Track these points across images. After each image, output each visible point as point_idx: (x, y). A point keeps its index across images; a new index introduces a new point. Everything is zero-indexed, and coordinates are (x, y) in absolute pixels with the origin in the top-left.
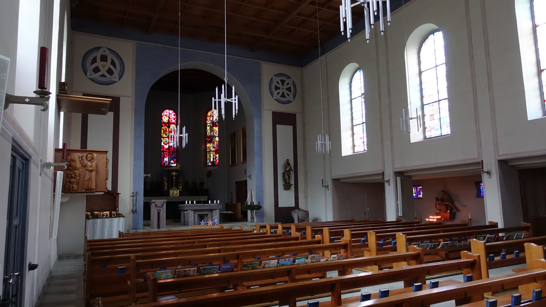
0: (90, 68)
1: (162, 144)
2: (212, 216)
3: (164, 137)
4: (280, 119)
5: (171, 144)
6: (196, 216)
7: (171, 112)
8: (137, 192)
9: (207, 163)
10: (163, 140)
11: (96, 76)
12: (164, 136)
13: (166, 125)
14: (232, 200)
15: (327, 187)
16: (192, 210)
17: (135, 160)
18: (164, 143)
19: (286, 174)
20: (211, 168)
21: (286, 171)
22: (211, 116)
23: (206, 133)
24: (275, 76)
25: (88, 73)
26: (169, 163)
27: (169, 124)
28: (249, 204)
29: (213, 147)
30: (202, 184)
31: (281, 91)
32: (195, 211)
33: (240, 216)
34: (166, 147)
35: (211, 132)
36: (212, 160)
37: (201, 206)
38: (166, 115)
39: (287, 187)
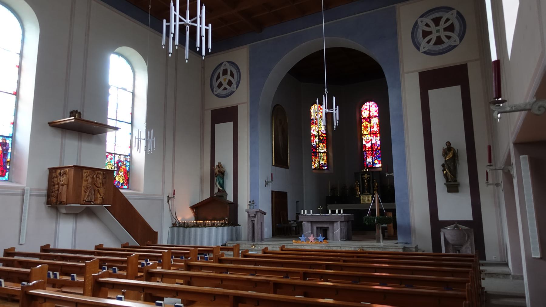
0: (216, 84)
1: (364, 143)
3: (365, 135)
4: (430, 80)
5: (373, 142)
6: (315, 229)
7: (371, 103)
8: (253, 201)
11: (220, 91)
12: (365, 133)
13: (366, 120)
15: (497, 185)
16: (308, 222)
17: (251, 166)
18: (366, 142)
19: (451, 166)
21: (445, 161)
24: (458, 13)
25: (214, 90)
26: (373, 163)
27: (370, 118)
31: (434, 37)
32: (312, 222)
34: (369, 145)
37: (323, 217)
38: (366, 109)
39: (453, 187)
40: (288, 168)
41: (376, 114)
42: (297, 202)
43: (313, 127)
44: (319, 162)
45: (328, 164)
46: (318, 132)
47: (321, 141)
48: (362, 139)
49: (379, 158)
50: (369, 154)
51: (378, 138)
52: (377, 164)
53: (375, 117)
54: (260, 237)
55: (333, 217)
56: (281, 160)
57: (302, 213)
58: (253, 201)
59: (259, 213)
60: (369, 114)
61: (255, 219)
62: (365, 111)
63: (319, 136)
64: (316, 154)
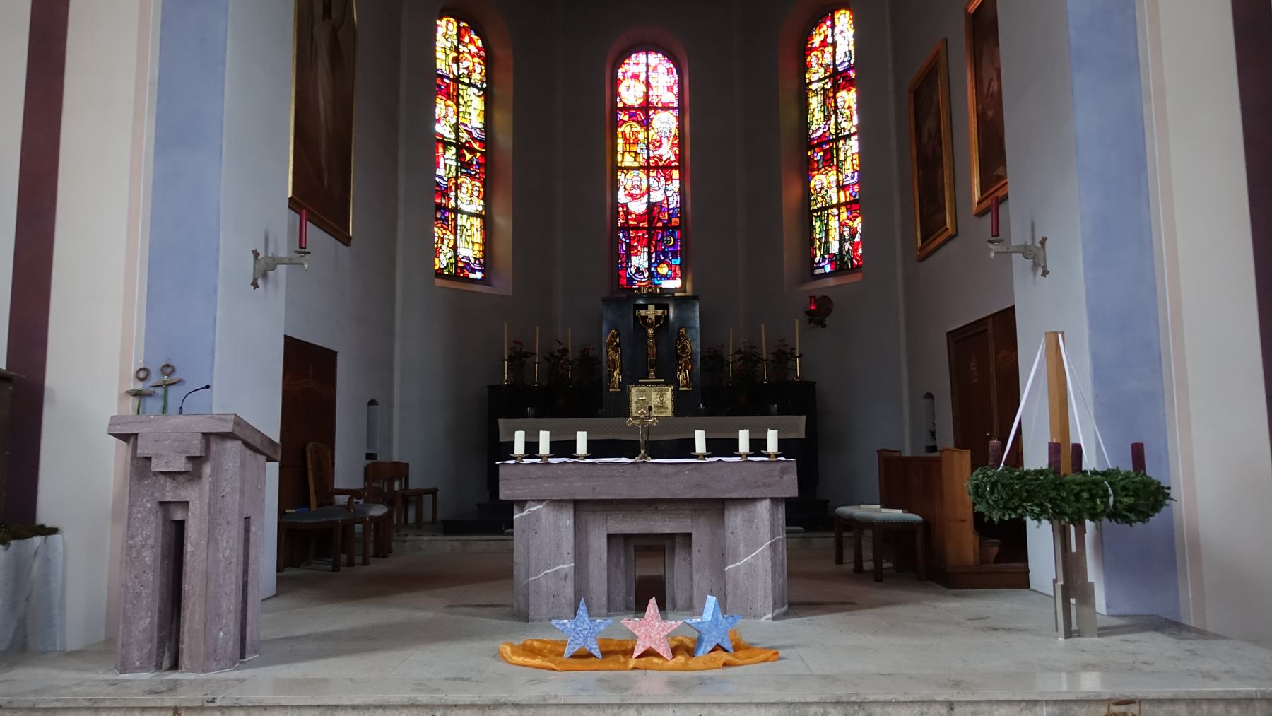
1: (622, 197)
2: (721, 557)
3: (629, 169)
5: (657, 197)
6: (598, 544)
7: (655, 59)
8: (168, 369)
9: (812, 265)
10: (625, 180)
12: (628, 161)
14: (933, 434)
16: (558, 503)
20: (831, 282)
22: (824, 44)
23: (806, 125)
27: (645, 111)
28: (1036, 458)
29: (841, 187)
30: (783, 357)
32: (580, 506)
33: (964, 543)
34: (638, 207)
35: (827, 118)
36: (834, 248)
37: (622, 476)
38: (635, 77)
40: (346, 240)
41: (670, 98)
42: (372, 403)
43: (442, 107)
44: (455, 248)
45: (487, 261)
46: (456, 128)
47: (464, 165)
48: (615, 186)
49: (675, 257)
50: (639, 240)
51: (676, 185)
52: (665, 277)
53: (666, 108)
54: (226, 633)
55: (724, 476)
56: (320, 194)
57: (519, 449)
58: (168, 369)
59: (234, 447)
60: (647, 96)
61: (198, 497)
62: (632, 82)
63: (460, 146)
64: (446, 215)
